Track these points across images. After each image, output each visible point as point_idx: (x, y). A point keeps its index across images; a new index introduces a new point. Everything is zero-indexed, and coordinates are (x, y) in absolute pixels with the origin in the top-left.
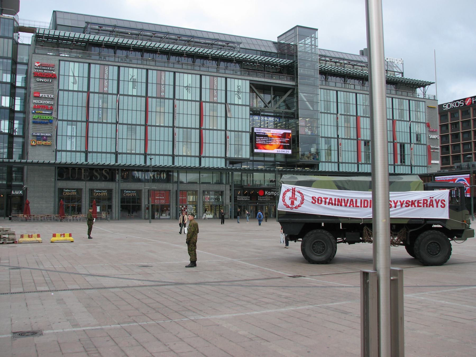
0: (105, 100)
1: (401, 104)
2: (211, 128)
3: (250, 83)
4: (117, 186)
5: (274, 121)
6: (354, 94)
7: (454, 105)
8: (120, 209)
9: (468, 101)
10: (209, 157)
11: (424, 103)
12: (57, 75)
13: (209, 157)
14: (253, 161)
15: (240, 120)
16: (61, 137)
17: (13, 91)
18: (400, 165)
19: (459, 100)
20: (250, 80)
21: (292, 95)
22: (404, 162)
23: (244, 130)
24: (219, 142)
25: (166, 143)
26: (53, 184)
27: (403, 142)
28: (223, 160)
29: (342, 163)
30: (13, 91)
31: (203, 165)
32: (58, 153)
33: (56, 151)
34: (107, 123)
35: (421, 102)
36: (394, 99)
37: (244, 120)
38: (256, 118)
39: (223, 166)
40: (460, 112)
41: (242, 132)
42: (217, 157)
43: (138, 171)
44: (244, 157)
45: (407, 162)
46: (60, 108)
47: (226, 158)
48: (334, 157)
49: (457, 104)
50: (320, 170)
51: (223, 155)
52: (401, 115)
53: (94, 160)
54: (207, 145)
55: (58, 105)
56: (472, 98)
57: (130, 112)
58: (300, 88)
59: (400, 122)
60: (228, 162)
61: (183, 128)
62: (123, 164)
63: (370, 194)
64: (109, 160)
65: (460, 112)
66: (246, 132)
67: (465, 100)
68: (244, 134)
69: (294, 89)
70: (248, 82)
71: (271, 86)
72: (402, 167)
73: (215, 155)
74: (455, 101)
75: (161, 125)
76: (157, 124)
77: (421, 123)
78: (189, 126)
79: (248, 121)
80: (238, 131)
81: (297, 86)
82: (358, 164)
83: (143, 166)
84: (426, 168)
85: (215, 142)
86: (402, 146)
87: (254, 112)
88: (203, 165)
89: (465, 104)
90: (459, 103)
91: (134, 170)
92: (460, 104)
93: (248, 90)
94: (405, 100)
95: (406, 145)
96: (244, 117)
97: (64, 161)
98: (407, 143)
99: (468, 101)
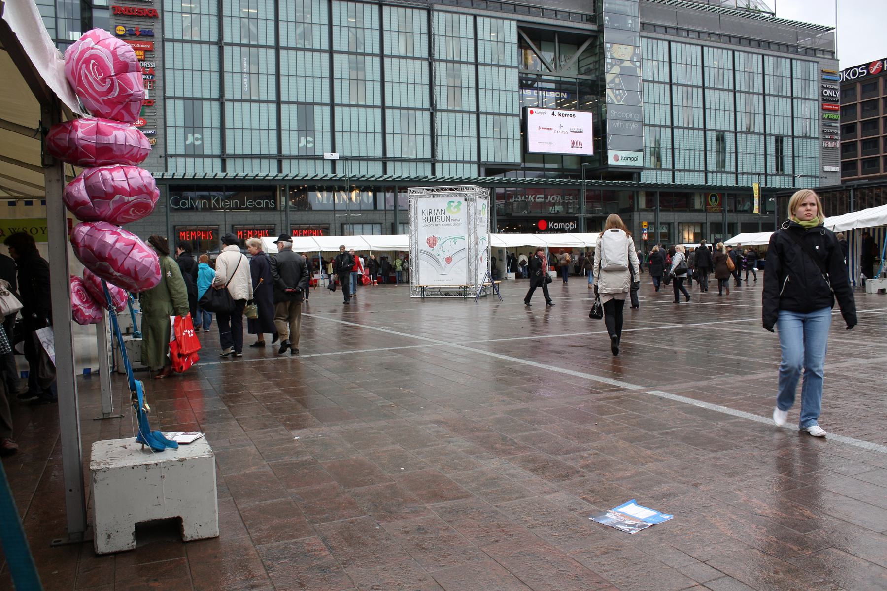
0: (253, 59)
1: (777, 66)
2: (450, 108)
3: (519, 27)
4: (284, 218)
5: (557, 99)
6: (699, 48)
7: (849, 75)
8: (412, 214)
9: (875, 68)
10: (449, 161)
11: (815, 64)
12: (159, 12)
13: (449, 161)
14: (525, 169)
15: (502, 94)
16: (173, 129)
17: (87, 15)
18: (775, 175)
19: (858, 67)
20: (518, 21)
21: (592, 46)
22: (782, 170)
23: (510, 111)
24: (466, 134)
25: (370, 136)
26: (164, 219)
27: (781, 133)
28: (475, 167)
29: (680, 171)
30: (87, 15)
31: (439, 175)
32: (169, 159)
33: (167, 156)
34: (259, 101)
35: (811, 64)
36: (766, 57)
37: (509, 94)
38: (528, 92)
39: (474, 175)
40: (859, 87)
41: (506, 115)
42: (464, 162)
43: (321, 189)
44: (511, 160)
45: (788, 169)
46: (168, 74)
47: (479, 163)
48: (666, 162)
49: (854, 74)
50: (643, 181)
51: (475, 158)
52: (778, 87)
53: (237, 170)
54: (445, 139)
55: (164, 69)
56: (882, 60)
57: (301, 80)
58: (607, 35)
59: (776, 98)
60: (483, 170)
61: (400, 108)
62: (291, 175)
63: (472, 273)
64: (267, 171)
65: (859, 87)
66: (513, 115)
67: (868, 65)
68: (510, 118)
69: (595, 38)
70: (514, 24)
71: (555, 32)
72: (778, 178)
73: (460, 158)
74: (851, 69)
75: (360, 103)
76: (353, 103)
77: (810, 100)
78: (411, 105)
79: (516, 95)
80: (500, 114)
81: (600, 31)
82: (706, 172)
83: (330, 179)
84: (817, 179)
85: (459, 134)
86: (779, 140)
87: (525, 83)
88: (439, 175)
89: (868, 72)
90: (859, 71)
91: (313, 189)
92: (860, 74)
93: (515, 39)
94: (784, 60)
95: (785, 139)
96: (509, 88)
97: (179, 174)
98: (788, 136)
99: (875, 68)
